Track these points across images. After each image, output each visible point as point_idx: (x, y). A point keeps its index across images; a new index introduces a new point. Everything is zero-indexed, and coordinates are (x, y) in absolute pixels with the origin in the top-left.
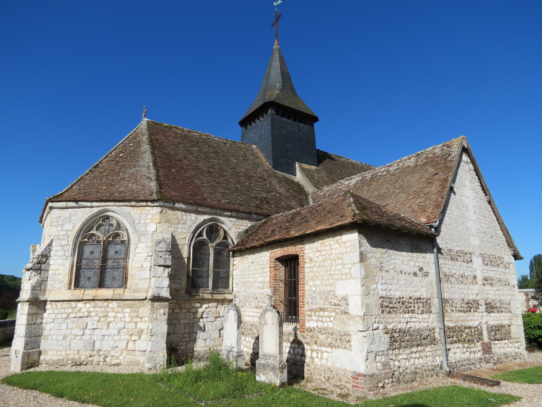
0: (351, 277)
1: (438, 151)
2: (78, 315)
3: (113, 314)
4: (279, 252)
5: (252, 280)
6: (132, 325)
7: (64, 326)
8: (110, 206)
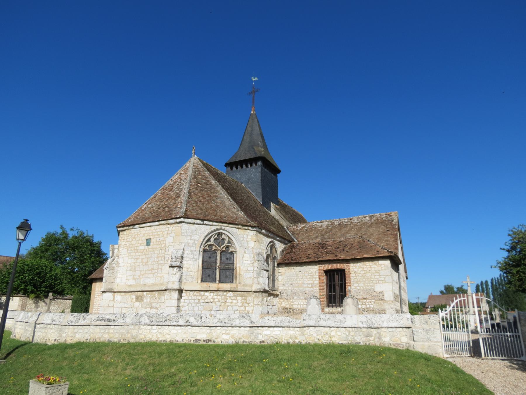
0: (386, 282)
1: (383, 216)
2: (206, 301)
3: (230, 301)
4: (328, 267)
5: (300, 282)
6: (243, 308)
7: (196, 309)
8: (225, 226)
